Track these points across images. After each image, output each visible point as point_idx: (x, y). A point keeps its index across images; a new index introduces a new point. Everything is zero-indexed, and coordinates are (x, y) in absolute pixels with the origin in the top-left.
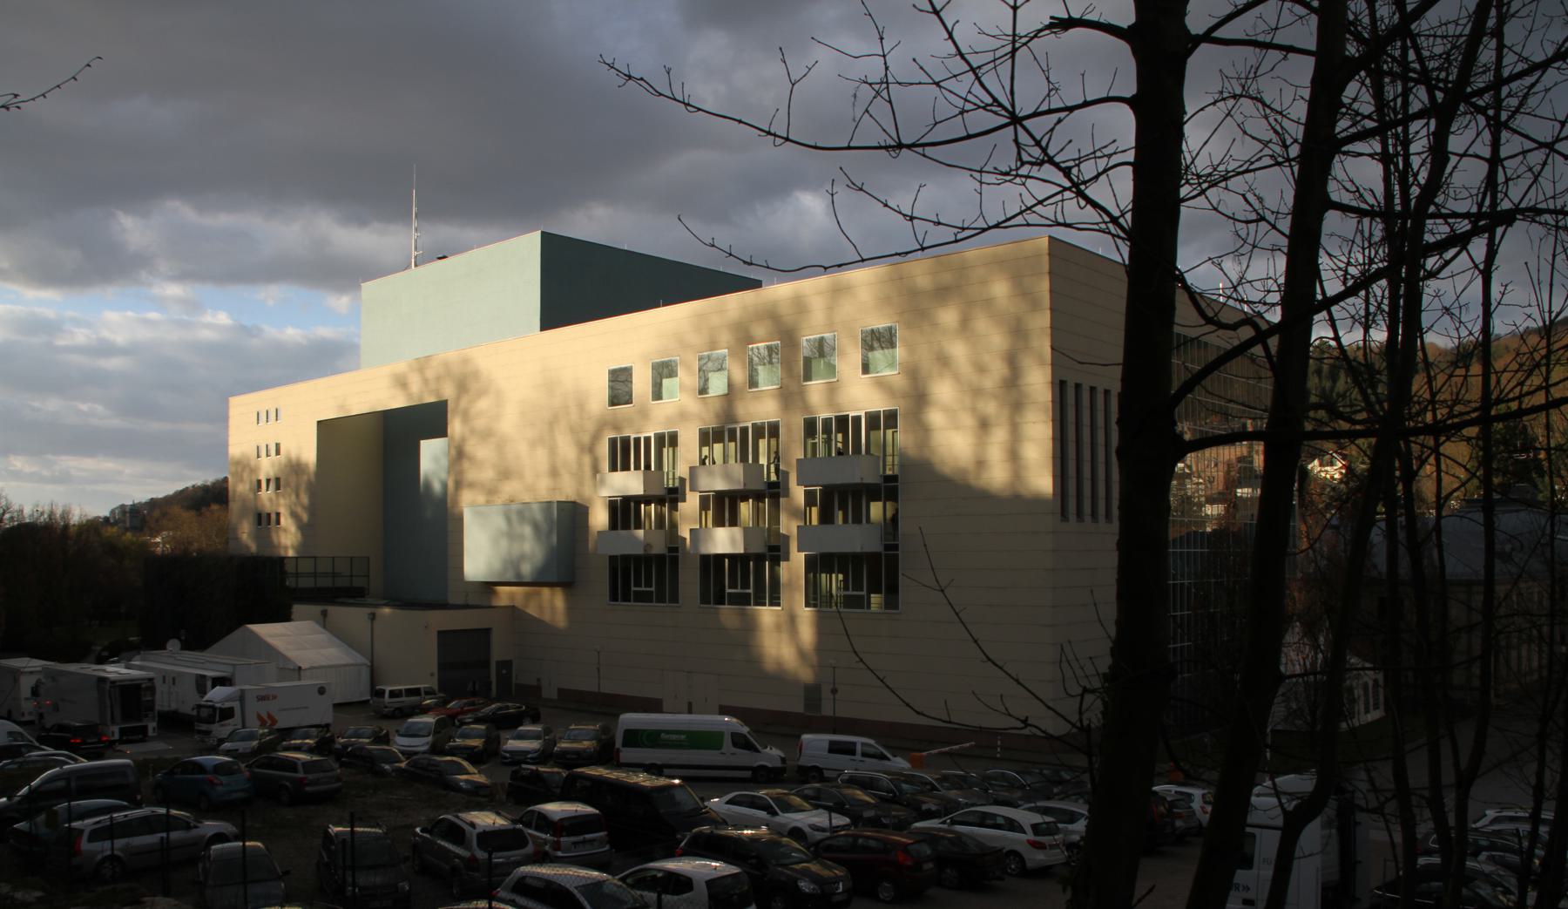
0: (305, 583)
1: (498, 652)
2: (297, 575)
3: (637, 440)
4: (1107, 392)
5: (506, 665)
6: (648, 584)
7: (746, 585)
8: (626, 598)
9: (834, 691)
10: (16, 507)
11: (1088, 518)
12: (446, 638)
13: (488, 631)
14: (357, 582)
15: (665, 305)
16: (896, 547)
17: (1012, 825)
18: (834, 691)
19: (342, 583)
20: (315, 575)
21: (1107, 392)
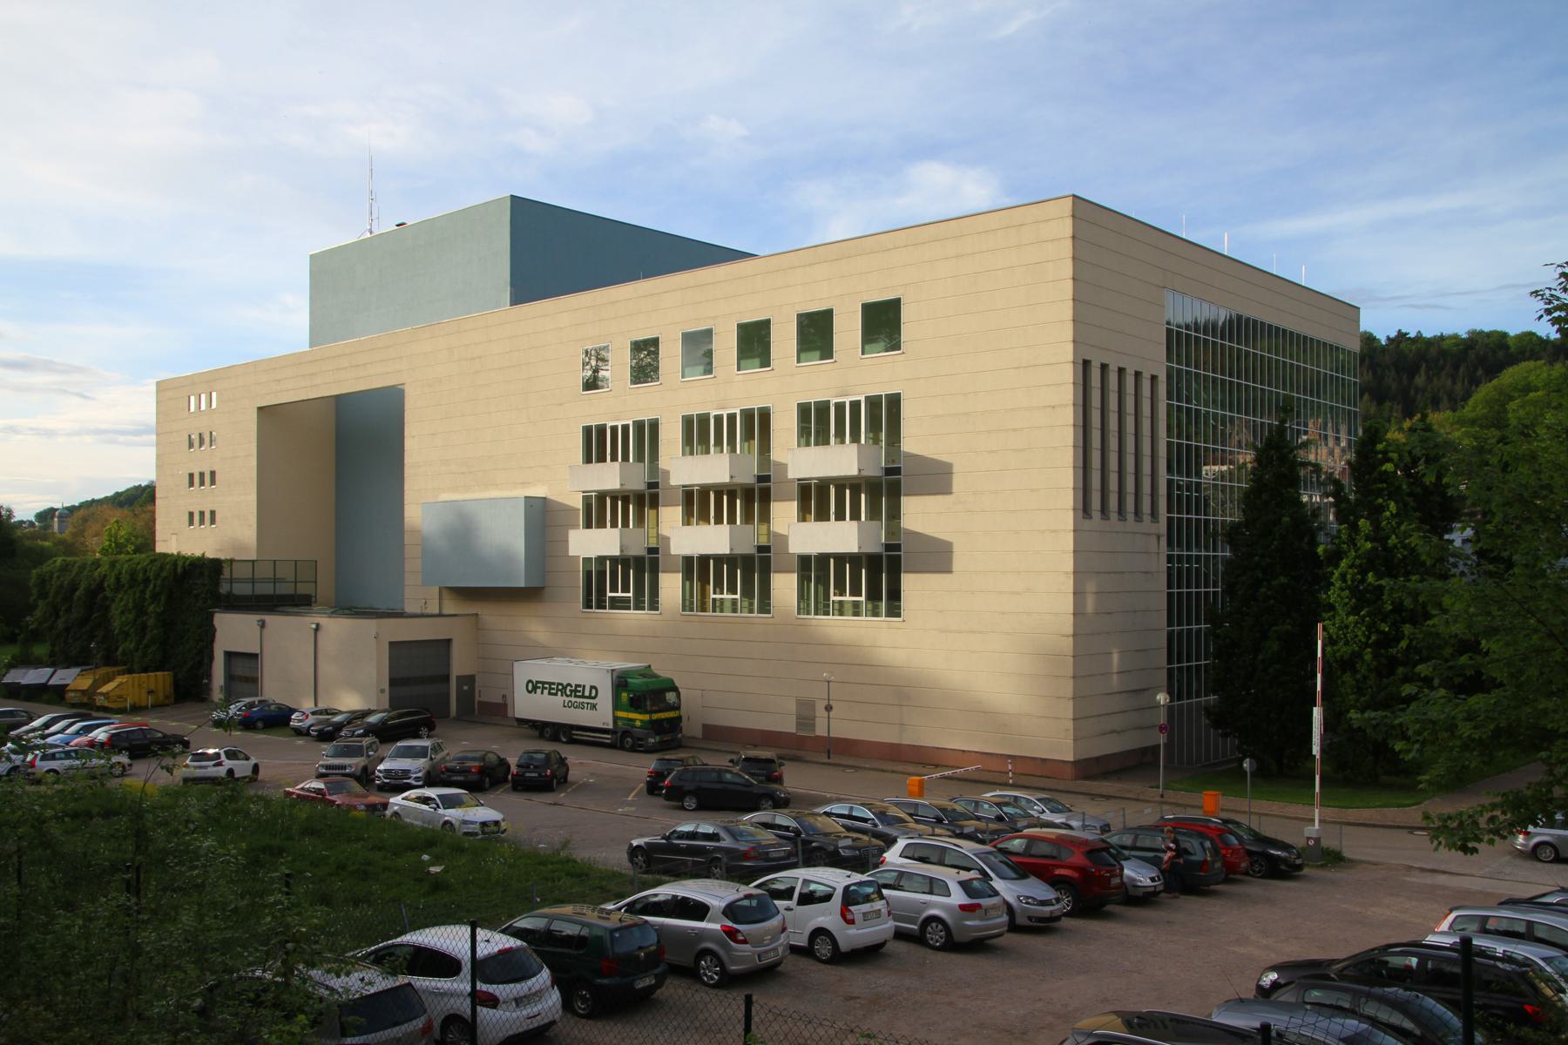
0: (241, 589)
1: (460, 664)
2: (231, 581)
3: (614, 429)
4: (1154, 378)
5: (469, 680)
6: (626, 589)
7: (625, 589)
8: (601, 606)
9: (829, 708)
10: (753, 551)
11: (1114, 516)
12: (398, 649)
13: (449, 641)
14: (303, 589)
15: (646, 276)
16: (898, 547)
17: (698, 910)
18: (829, 708)
19: (285, 589)
20: (253, 581)
21: (1154, 378)
